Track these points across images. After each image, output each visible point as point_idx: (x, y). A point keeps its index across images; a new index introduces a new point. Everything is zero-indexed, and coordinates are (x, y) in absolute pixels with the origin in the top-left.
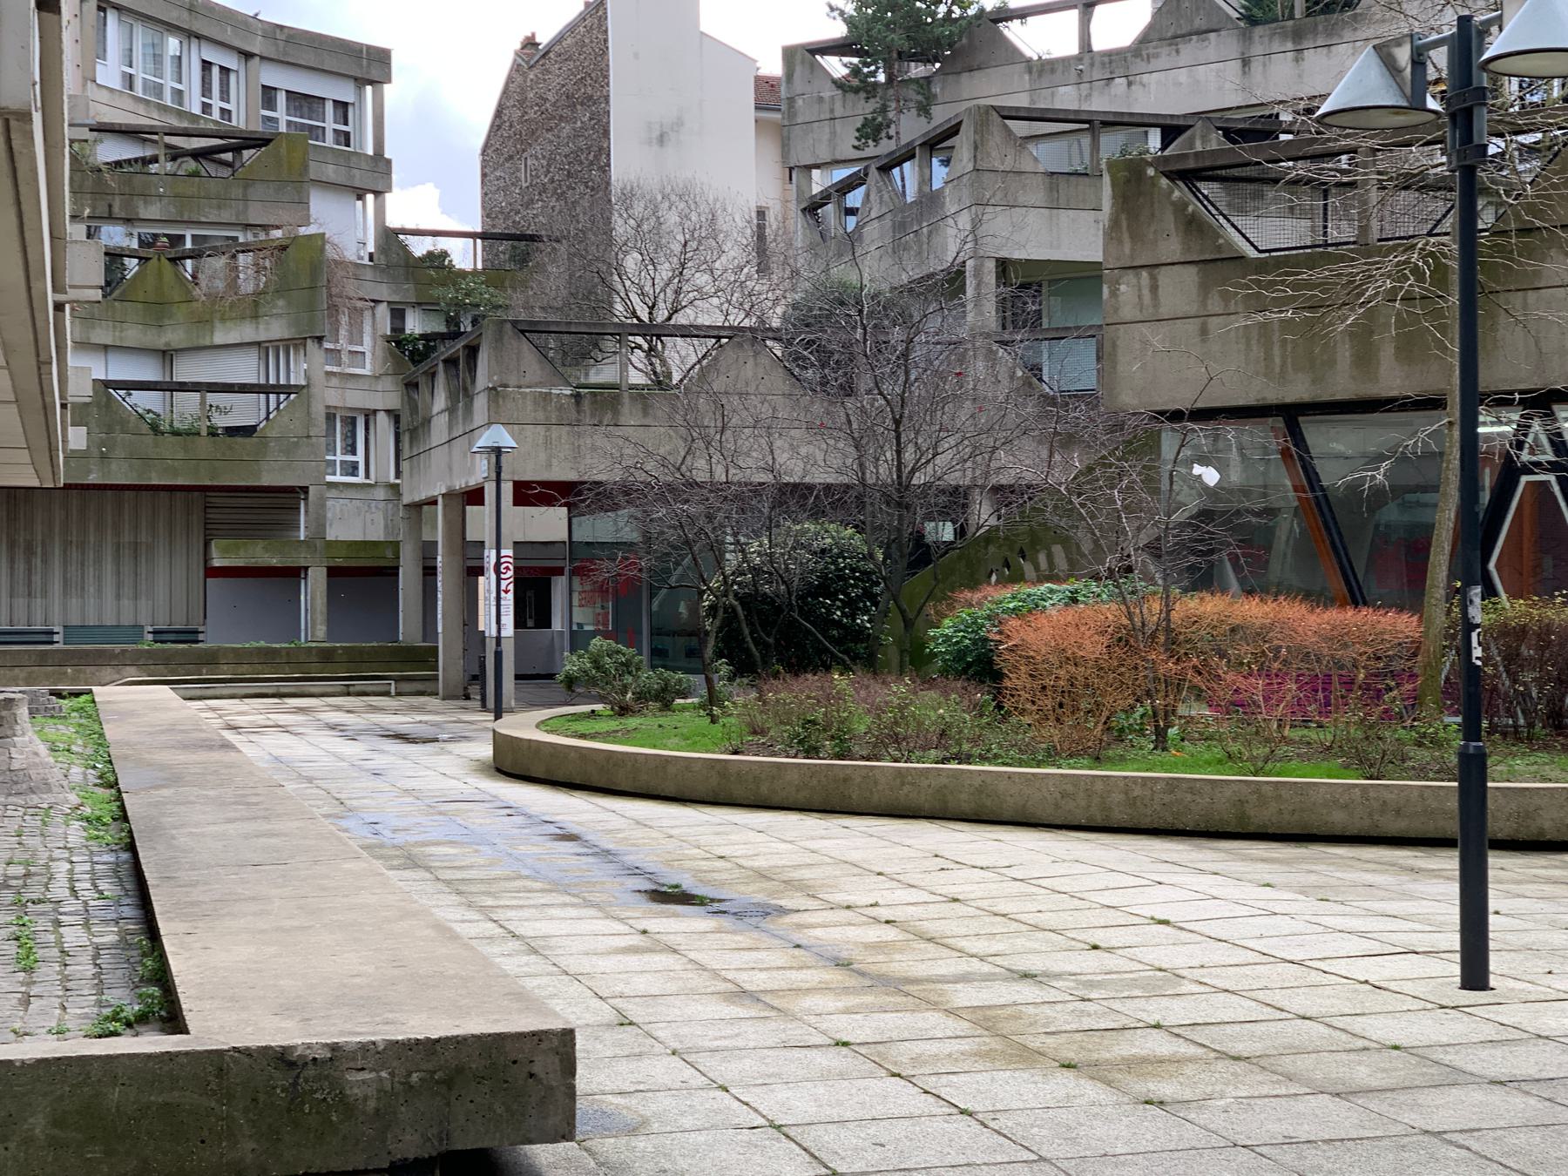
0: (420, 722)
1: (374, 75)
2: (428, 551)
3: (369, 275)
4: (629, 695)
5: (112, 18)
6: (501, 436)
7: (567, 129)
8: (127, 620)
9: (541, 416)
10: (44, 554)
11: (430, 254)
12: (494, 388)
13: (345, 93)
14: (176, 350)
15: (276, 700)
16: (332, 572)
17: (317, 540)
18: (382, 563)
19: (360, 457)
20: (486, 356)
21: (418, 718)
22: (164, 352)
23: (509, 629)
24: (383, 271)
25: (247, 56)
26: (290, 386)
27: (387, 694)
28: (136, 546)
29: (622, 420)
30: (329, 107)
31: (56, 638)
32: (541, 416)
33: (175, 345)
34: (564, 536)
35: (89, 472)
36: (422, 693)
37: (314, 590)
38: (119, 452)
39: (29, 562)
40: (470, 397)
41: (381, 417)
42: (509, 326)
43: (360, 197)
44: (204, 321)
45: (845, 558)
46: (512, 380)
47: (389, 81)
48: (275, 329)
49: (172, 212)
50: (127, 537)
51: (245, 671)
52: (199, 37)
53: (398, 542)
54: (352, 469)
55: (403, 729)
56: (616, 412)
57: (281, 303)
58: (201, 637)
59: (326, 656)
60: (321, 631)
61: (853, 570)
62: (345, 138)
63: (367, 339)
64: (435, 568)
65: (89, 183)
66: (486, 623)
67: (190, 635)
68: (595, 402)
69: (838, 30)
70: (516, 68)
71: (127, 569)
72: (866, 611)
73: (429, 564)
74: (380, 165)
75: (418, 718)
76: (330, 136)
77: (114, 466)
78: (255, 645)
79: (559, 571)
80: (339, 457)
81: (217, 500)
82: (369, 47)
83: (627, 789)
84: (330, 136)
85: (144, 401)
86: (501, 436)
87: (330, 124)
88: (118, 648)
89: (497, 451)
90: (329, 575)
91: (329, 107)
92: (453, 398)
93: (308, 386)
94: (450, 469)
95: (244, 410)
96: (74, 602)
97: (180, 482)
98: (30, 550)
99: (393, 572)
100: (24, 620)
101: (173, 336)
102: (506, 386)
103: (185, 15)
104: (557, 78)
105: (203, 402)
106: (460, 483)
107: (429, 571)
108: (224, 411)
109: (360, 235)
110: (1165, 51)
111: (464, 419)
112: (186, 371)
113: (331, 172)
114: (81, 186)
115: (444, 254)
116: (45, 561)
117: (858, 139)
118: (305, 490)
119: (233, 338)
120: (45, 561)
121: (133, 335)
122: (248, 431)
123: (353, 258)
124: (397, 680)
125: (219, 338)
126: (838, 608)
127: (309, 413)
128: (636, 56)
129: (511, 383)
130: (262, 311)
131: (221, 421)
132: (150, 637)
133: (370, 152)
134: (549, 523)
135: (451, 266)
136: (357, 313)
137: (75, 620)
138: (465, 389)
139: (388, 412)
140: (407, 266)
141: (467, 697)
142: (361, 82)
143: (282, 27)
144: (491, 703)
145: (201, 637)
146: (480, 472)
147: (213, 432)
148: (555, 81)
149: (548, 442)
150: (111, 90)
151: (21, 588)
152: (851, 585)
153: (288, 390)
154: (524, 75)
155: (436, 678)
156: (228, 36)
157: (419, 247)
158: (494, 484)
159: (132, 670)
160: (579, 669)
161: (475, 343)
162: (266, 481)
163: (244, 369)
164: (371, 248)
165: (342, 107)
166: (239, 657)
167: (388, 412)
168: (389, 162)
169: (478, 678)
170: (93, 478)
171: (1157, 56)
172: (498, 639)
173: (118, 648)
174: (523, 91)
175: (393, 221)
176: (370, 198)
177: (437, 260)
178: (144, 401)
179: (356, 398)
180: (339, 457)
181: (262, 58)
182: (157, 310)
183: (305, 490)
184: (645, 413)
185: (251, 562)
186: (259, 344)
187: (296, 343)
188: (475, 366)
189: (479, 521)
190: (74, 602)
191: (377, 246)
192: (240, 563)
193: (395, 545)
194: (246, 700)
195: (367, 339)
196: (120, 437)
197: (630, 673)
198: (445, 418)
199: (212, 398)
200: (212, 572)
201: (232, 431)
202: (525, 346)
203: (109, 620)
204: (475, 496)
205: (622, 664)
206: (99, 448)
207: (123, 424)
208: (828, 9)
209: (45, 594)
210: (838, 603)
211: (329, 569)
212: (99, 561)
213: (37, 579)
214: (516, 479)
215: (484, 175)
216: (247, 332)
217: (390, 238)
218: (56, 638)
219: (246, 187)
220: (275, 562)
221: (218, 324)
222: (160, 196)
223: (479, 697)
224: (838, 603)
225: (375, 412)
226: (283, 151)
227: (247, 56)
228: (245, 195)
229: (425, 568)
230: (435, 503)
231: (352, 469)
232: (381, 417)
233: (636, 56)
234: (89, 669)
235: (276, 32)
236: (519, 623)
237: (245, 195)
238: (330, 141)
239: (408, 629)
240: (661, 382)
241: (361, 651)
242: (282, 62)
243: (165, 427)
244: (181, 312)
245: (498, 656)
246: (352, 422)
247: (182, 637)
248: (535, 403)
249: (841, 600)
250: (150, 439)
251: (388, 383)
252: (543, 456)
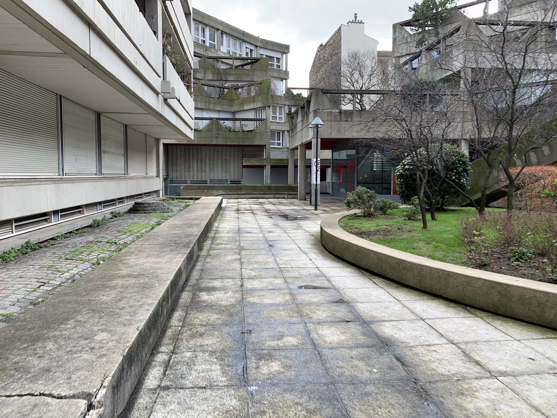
0: (292, 209)
1: (286, 51)
2: (296, 161)
3: (283, 99)
4: (372, 209)
5: (224, 36)
6: (318, 121)
7: (330, 62)
8: (224, 178)
9: (329, 118)
10: (205, 162)
11: (297, 94)
12: (315, 110)
13: (278, 55)
14: (236, 112)
15: (256, 200)
16: (272, 167)
17: (268, 159)
18: (285, 164)
19: (281, 142)
20: (313, 101)
21: (292, 208)
22: (233, 112)
23: (319, 182)
24: (287, 98)
25: (256, 46)
26: (262, 119)
27: (284, 198)
28: (226, 160)
29: (354, 120)
30: (275, 59)
31: (208, 182)
32: (329, 118)
33: (235, 111)
34: (331, 158)
35: (213, 141)
36: (294, 198)
37: (267, 171)
38: (220, 136)
39: (201, 164)
40: (308, 115)
41: (286, 132)
42: (320, 91)
43: (282, 81)
44: (242, 104)
45: (455, 156)
46: (321, 107)
47: (289, 53)
48: (259, 105)
49: (236, 79)
50: (224, 158)
51: (250, 192)
52: (245, 41)
53: (288, 159)
54: (279, 144)
55: (287, 212)
56: (352, 117)
57: (260, 98)
58: (241, 182)
59: (269, 188)
60: (269, 181)
61: (459, 161)
62: (279, 66)
63: (283, 115)
64: (297, 166)
65: (216, 72)
66: (313, 182)
67: (239, 182)
68: (345, 114)
69: (409, 16)
70: (318, 51)
71: (224, 166)
72: (464, 177)
73: (296, 165)
74: (286, 73)
75: (292, 208)
76: (275, 66)
77: (219, 140)
78: (252, 185)
79: (329, 167)
80: (276, 142)
81: (245, 149)
82: (285, 45)
83: (413, 285)
84: (275, 66)
85: (228, 124)
86: (318, 121)
87: (275, 63)
88: (217, 185)
89: (317, 126)
90: (271, 168)
91: (275, 59)
92: (303, 117)
93: (266, 119)
94: (302, 137)
95: (250, 126)
96: (212, 174)
97: (235, 144)
98: (201, 161)
99: (286, 167)
100: (200, 178)
101: (235, 108)
102: (319, 109)
103: (242, 36)
104: (328, 50)
105: (241, 123)
106: (304, 141)
107: (296, 167)
108: (246, 126)
109: (282, 90)
110: (517, 10)
111: (306, 121)
112: (238, 116)
113: (275, 74)
114: (214, 72)
115: (301, 94)
116: (205, 164)
117: (416, 45)
118: (265, 145)
119: (248, 108)
120: (205, 164)
121: (226, 108)
122: (251, 131)
123: (280, 95)
124: (287, 195)
125: (245, 108)
126: (454, 175)
127: (266, 126)
128: (348, 41)
129: (321, 109)
130: (255, 99)
131: (246, 129)
132: (230, 182)
133: (284, 69)
134: (327, 154)
135: (302, 97)
136: (280, 108)
137: (212, 178)
138: (307, 114)
139: (287, 131)
140: (292, 96)
141: (306, 200)
142: (283, 53)
143: (264, 40)
144: (313, 203)
145: (241, 182)
146: (310, 135)
147: (243, 132)
148: (327, 52)
149: (331, 126)
150: (224, 53)
151: (200, 170)
152: (458, 167)
153: (261, 120)
154: (320, 52)
155: (297, 194)
156: (252, 41)
157: (295, 92)
158: (316, 139)
159: (221, 191)
160: (353, 199)
161: (310, 99)
162: (256, 143)
163: (251, 115)
164: (284, 93)
165: (278, 59)
166: (248, 188)
167: (287, 131)
168: (288, 72)
169: (309, 193)
170: (214, 143)
171: (514, 12)
172: (316, 185)
173: (217, 185)
174: (320, 56)
175: (289, 86)
176: (284, 81)
177: (299, 95)
178: (228, 124)
179: (280, 128)
180: (276, 142)
181: (260, 47)
182: (231, 102)
183: (265, 145)
184: (361, 117)
185: (252, 164)
186: (254, 109)
187: (263, 108)
188: (310, 106)
189: (310, 154)
190: (212, 174)
191: (286, 92)
192: (249, 164)
193: (287, 160)
194: (249, 199)
195: (283, 115)
196: (220, 132)
197: (372, 200)
198: (301, 123)
199: (243, 122)
200: (244, 167)
201: (248, 131)
202: (325, 97)
203: (220, 178)
204: (308, 146)
205: (369, 197)
206: (216, 135)
207: (221, 128)
208: (409, 9)
209: (205, 172)
210: (454, 174)
211: (271, 166)
212: (217, 164)
213: (203, 168)
214: (321, 137)
215: (310, 78)
216: (252, 106)
217: (288, 90)
218: (208, 182)
219: (253, 72)
220: (258, 164)
221: (245, 104)
222: (233, 74)
223: (309, 200)
224: (454, 174)
225: (284, 131)
226: (262, 62)
227: (256, 46)
228: (253, 73)
229: (295, 166)
230: (297, 149)
231: (279, 144)
232: (286, 132)
233: (348, 41)
234: (210, 191)
235: (263, 41)
236: (321, 180)
237: (253, 73)
238: (275, 67)
239: (290, 181)
240: (363, 110)
241: (278, 187)
242: (264, 48)
243: (232, 130)
244: (237, 102)
245: (316, 190)
246: (279, 133)
247: (199, 182)
248: (328, 115)
249: (455, 172)
250: (227, 133)
251: (287, 124)
252: (329, 131)
